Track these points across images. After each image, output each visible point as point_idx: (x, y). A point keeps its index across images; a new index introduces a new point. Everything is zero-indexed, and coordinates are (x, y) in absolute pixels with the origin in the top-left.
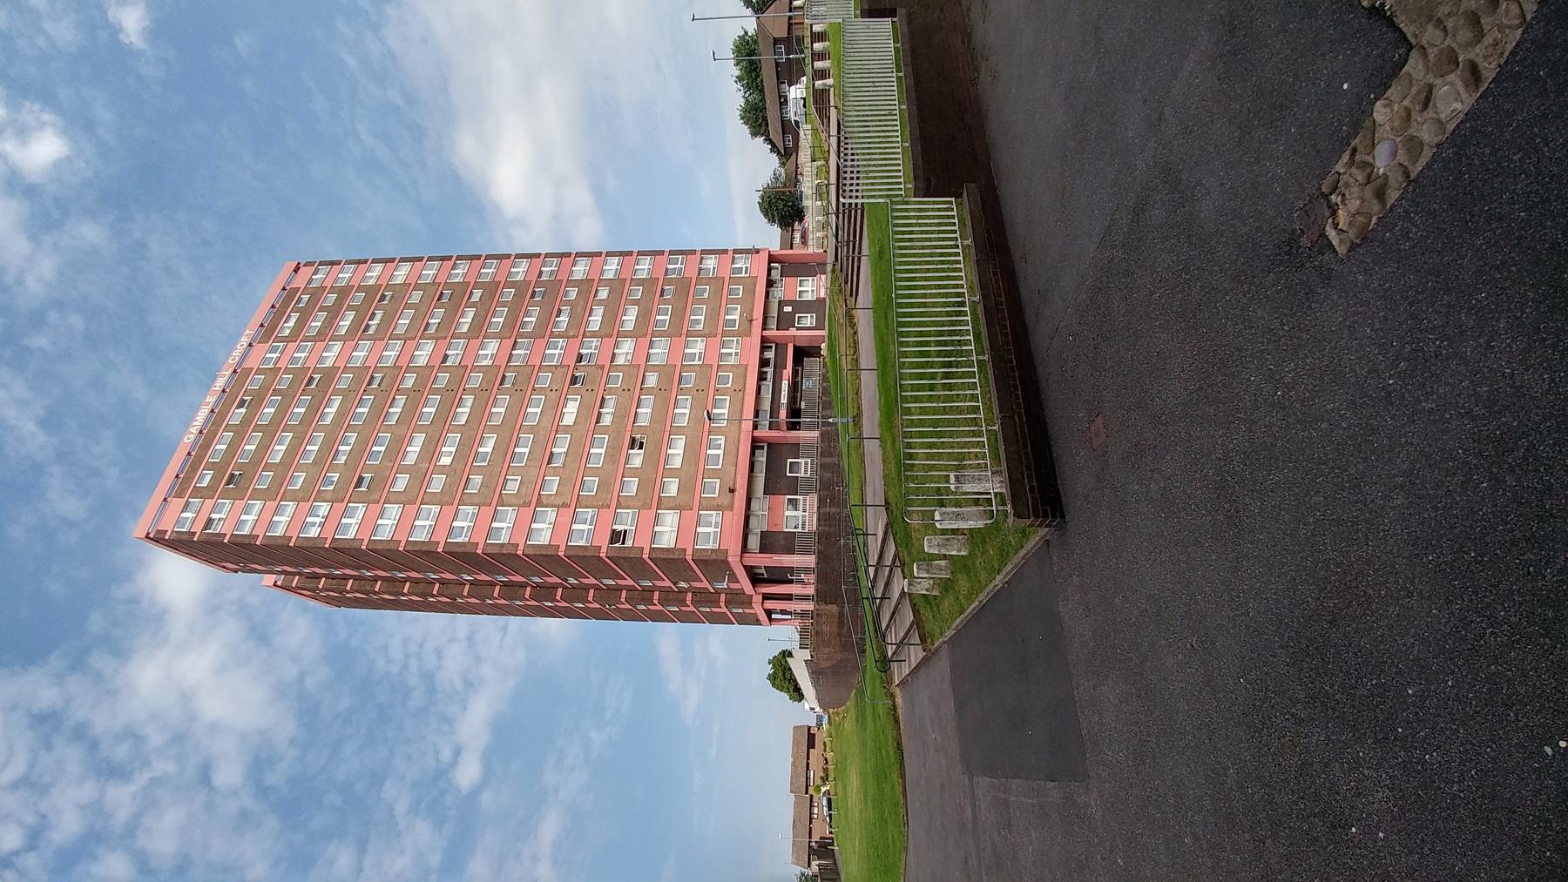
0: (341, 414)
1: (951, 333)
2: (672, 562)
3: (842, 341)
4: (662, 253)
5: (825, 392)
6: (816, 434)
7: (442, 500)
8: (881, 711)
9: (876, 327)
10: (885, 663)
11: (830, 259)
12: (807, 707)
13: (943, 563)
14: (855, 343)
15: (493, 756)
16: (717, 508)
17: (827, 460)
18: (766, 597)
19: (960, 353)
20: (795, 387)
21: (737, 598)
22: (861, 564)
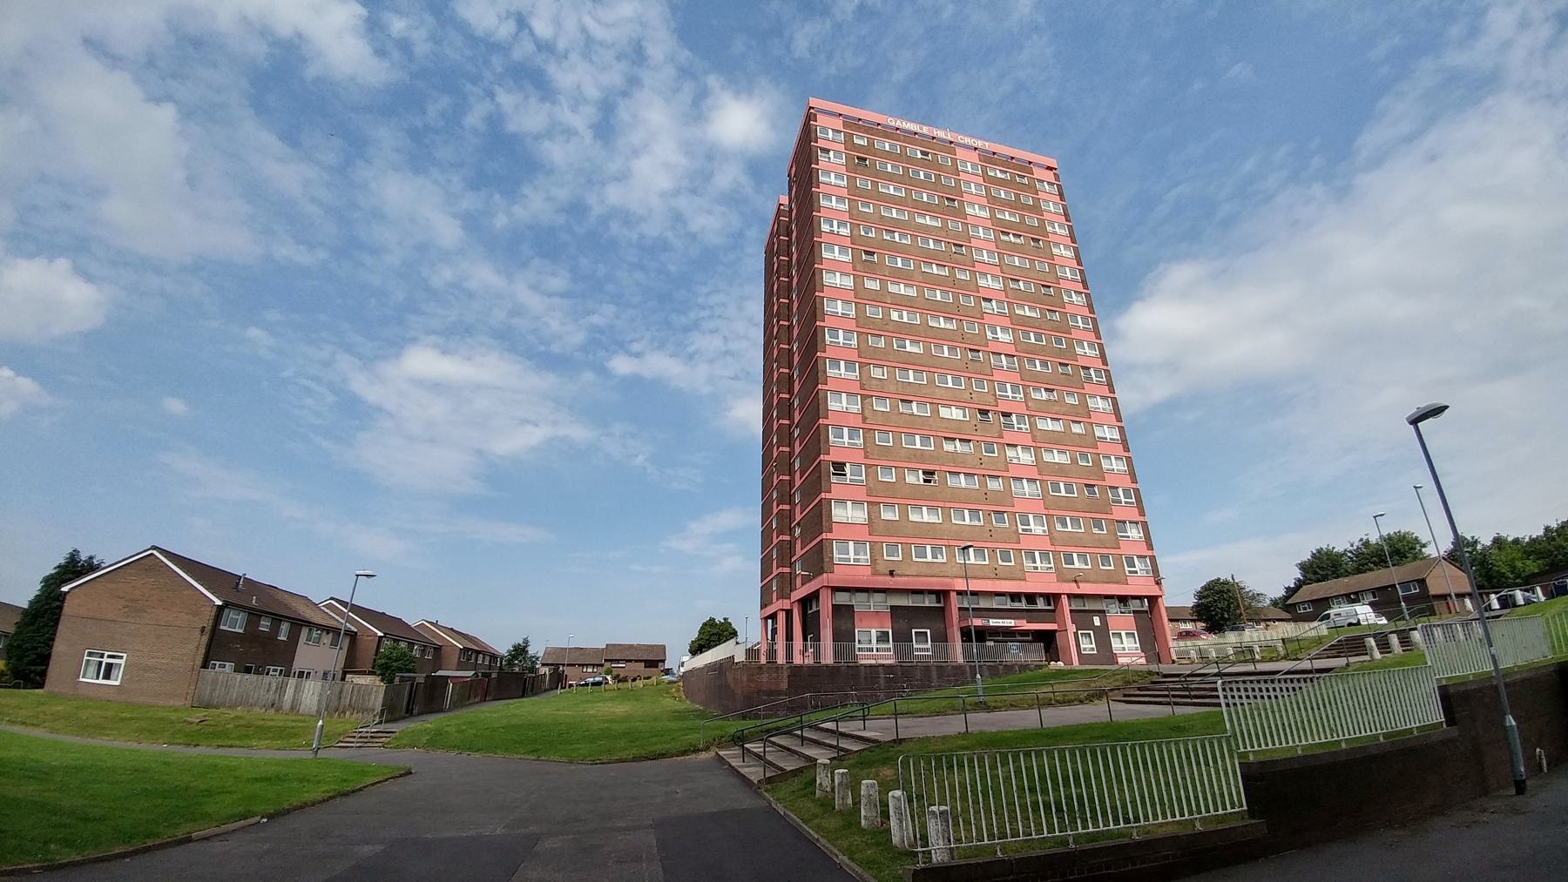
0: (926, 229)
1: (1093, 810)
2: (818, 520)
3: (1069, 687)
4: (1134, 481)
5: (1009, 669)
6: (960, 660)
7: (861, 319)
8: (692, 737)
9: (1090, 727)
10: (739, 740)
11: (1165, 668)
12: (685, 659)
13: (850, 801)
14: (1069, 702)
15: (633, 384)
16: (873, 560)
17: (934, 674)
18: (789, 613)
19: (1073, 821)
20: (1008, 633)
21: (787, 583)
22: (840, 712)
